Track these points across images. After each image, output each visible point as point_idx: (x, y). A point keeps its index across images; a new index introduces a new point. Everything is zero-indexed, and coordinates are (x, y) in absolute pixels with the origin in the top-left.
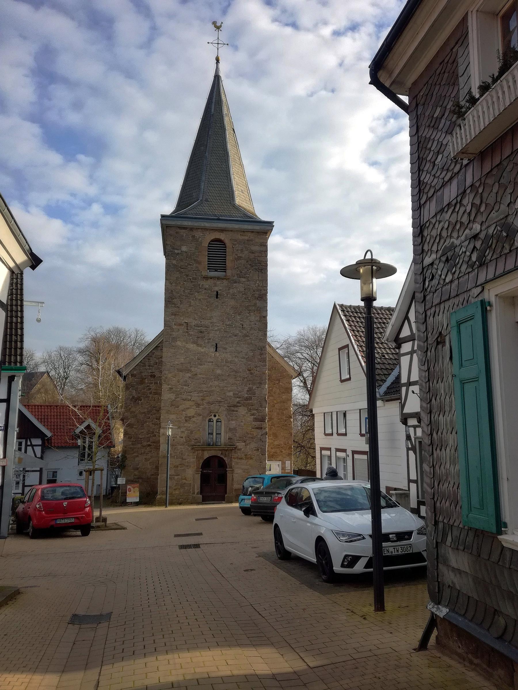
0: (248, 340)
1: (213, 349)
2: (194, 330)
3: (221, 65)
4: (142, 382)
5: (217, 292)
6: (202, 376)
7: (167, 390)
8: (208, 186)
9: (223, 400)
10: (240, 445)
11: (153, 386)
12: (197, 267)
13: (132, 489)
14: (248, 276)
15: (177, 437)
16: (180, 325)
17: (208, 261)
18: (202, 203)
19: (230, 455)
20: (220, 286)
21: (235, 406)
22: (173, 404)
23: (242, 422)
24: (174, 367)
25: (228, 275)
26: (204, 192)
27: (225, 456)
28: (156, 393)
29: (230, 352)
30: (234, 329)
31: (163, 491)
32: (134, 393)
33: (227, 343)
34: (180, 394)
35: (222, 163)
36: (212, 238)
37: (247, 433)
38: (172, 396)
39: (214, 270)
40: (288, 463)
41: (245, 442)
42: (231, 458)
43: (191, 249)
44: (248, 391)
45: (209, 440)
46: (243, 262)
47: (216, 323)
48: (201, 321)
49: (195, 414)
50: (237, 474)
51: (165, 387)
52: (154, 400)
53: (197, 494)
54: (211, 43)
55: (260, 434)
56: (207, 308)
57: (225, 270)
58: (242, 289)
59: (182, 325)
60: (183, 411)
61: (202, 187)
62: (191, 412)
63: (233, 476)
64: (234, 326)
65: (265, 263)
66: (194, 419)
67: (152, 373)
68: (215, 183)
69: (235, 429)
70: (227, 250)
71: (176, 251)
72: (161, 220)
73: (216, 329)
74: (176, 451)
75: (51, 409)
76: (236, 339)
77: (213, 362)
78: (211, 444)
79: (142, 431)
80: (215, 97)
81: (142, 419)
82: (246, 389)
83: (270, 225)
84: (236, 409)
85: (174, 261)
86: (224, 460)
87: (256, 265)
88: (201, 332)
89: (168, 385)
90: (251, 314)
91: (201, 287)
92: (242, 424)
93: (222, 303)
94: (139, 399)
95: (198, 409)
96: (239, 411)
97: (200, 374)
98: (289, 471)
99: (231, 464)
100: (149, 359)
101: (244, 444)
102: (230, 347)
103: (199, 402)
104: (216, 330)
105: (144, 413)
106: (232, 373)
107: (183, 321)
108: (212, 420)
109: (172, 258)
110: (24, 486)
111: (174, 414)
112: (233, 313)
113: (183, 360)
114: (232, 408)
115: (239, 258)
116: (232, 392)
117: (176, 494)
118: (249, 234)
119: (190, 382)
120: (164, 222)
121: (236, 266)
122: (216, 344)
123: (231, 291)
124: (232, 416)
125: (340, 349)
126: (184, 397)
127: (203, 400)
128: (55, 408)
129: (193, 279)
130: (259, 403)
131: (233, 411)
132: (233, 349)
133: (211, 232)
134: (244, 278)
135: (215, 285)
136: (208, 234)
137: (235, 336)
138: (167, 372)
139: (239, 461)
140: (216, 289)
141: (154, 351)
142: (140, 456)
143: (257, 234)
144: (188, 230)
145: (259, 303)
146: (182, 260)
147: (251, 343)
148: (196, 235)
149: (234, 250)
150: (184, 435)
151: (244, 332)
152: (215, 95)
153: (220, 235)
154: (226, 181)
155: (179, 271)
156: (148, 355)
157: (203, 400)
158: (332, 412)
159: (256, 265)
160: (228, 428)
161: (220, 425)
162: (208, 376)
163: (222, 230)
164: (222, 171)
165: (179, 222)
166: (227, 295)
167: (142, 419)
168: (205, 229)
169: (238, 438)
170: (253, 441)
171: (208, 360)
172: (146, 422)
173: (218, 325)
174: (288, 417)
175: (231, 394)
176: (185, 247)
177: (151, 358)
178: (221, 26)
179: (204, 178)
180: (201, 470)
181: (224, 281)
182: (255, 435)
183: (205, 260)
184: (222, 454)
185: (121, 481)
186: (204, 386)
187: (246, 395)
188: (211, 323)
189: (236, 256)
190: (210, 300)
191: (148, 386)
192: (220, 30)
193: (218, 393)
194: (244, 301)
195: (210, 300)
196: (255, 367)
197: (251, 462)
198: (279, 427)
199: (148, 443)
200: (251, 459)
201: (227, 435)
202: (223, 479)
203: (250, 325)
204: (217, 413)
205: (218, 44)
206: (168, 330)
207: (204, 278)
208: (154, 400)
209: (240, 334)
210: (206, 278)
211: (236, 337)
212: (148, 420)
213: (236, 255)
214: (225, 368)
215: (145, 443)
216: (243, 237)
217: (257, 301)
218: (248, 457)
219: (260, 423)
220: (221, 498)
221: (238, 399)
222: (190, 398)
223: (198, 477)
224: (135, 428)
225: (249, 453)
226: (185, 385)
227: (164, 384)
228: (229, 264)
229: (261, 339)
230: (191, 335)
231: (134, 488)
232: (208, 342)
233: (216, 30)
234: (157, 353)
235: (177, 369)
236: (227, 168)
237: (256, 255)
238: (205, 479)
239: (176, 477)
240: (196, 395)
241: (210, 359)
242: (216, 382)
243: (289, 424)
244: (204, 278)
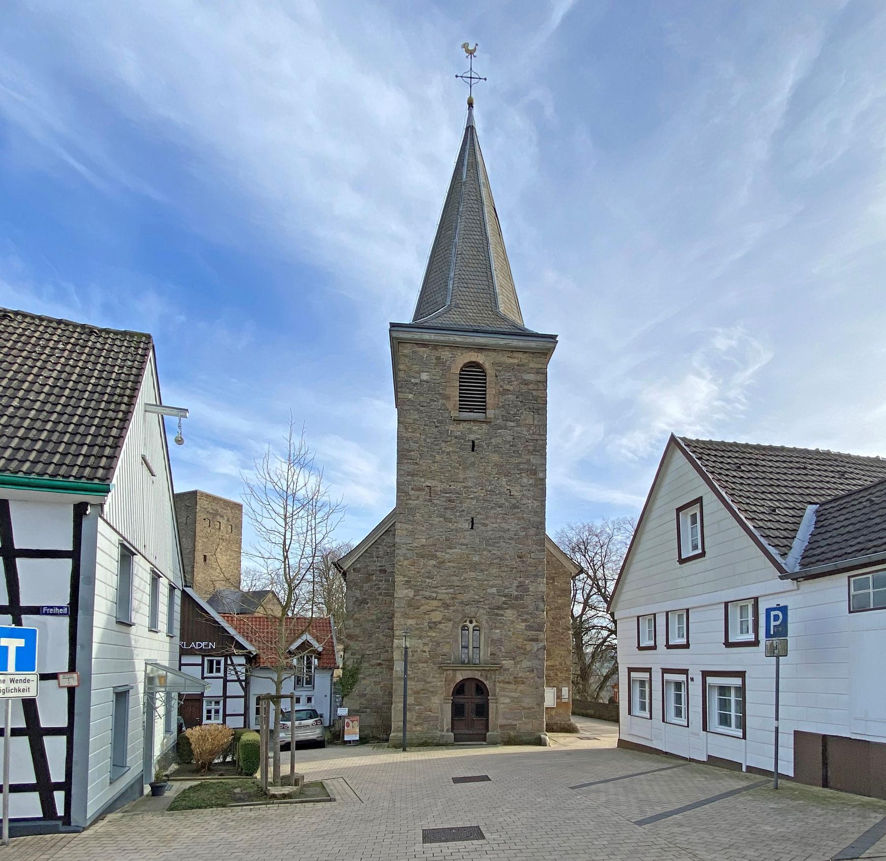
0: (518, 513)
1: (467, 526)
2: (439, 497)
3: (475, 111)
4: (368, 578)
5: (473, 442)
6: (451, 564)
7: (403, 584)
9: (482, 600)
10: (507, 663)
11: (383, 585)
12: (444, 404)
13: (351, 723)
14: (518, 418)
15: (417, 651)
16: (420, 489)
17: (460, 397)
18: (450, 310)
19: (493, 677)
20: (477, 432)
21: (498, 608)
22: (411, 604)
23: (509, 631)
24: (412, 550)
25: (488, 416)
26: (453, 295)
27: (487, 679)
28: (387, 595)
29: (491, 531)
30: (499, 496)
31: (399, 727)
32: (358, 593)
33: (487, 517)
34: (421, 590)
35: (479, 253)
37: (518, 647)
38: (411, 593)
39: (468, 410)
40: (565, 691)
41: (514, 659)
42: (495, 682)
43: (434, 377)
44: (518, 587)
45: (463, 656)
47: (471, 487)
48: (450, 484)
49: (442, 619)
50: (503, 703)
51: (399, 579)
52: (386, 604)
53: (447, 731)
55: (536, 649)
56: (458, 465)
57: (484, 410)
58: (509, 438)
59: (423, 490)
60: (425, 614)
61: (451, 286)
62: (437, 616)
63: (497, 707)
64: (497, 492)
65: (543, 400)
66: (442, 626)
67: (382, 566)
69: (499, 640)
70: (487, 380)
71: (413, 380)
72: (390, 331)
73: (472, 496)
74: (416, 670)
75: (260, 621)
76: (501, 512)
77: (467, 545)
78: (466, 662)
79: (370, 645)
80: (467, 157)
81: (369, 629)
82: (516, 583)
83: (552, 339)
84: (501, 612)
85: (411, 395)
86: (485, 685)
88: (450, 501)
89: (404, 576)
90: (523, 475)
91: (449, 434)
92: (510, 633)
93: (481, 458)
94: (364, 602)
95: (446, 611)
96: (505, 615)
97: (449, 562)
98: (566, 701)
99: (495, 690)
100: (378, 548)
101: (512, 662)
102: (493, 523)
103: (448, 602)
104: (471, 498)
105: (372, 621)
106: (495, 561)
107: (424, 485)
108: (466, 628)
109: (408, 390)
110: (225, 715)
111: (412, 618)
112: (496, 474)
113: (424, 540)
114: (495, 611)
116: (495, 589)
117: (417, 731)
118: (520, 355)
119: (436, 573)
120: (395, 334)
121: (501, 404)
122: (472, 518)
123: (493, 441)
124: (495, 623)
125: (679, 510)
126: (427, 594)
127: (453, 598)
128: (266, 620)
129: (438, 423)
130: (534, 604)
131: (497, 615)
132: (496, 525)
133: (464, 352)
135: (471, 431)
136: (459, 354)
137: (499, 507)
138: (402, 558)
139: (507, 686)
140: (472, 437)
141: (384, 537)
142: (368, 678)
143: (532, 355)
144: (430, 348)
145: (534, 460)
146: (421, 394)
147: (523, 518)
149: (497, 380)
150: (427, 649)
151: (513, 501)
153: (478, 356)
154: (485, 279)
155: (418, 410)
156: (375, 542)
157: (453, 598)
158: (655, 615)
160: (490, 639)
162: (461, 565)
163: (481, 349)
164: (480, 265)
165: (417, 335)
166: (488, 446)
167: (369, 629)
168: (455, 347)
169: (504, 654)
170: (525, 658)
171: (460, 542)
172: (375, 633)
173: (475, 490)
174: (565, 629)
175: (494, 590)
176: (426, 374)
177: (380, 546)
179: (452, 275)
180: (452, 698)
181: (484, 426)
182: (528, 649)
183: (455, 393)
184: (481, 676)
185: (342, 712)
186: (455, 578)
187: (516, 593)
188: (465, 487)
190: (463, 453)
191: (376, 585)
192: (475, 56)
193: (475, 589)
194: (513, 456)
195: (463, 453)
196: (528, 553)
197: (521, 687)
198: (554, 641)
199: (379, 661)
200: (522, 683)
201: (489, 649)
202: (482, 711)
203: (521, 491)
204: (474, 617)
205: (471, 78)
206: (402, 498)
207: (454, 420)
208: (386, 604)
209: (507, 504)
210: (458, 421)
211: (500, 509)
212: (377, 630)
213: (501, 387)
214: (485, 553)
215: (374, 662)
216: (512, 361)
218: (517, 681)
219: (535, 633)
220: (481, 738)
221: (504, 599)
222: (434, 595)
223: (448, 708)
224: (360, 641)
225: (520, 675)
226: (428, 577)
227: (398, 575)
228: (490, 400)
229: (536, 512)
230: (436, 505)
231: (353, 721)
232: (461, 516)
233: (467, 57)
234: (388, 539)
235: (416, 553)
237: (531, 387)
238: (458, 711)
239: (417, 708)
240: (444, 591)
241: (464, 540)
242: (472, 573)
243: (567, 639)
244: (454, 420)
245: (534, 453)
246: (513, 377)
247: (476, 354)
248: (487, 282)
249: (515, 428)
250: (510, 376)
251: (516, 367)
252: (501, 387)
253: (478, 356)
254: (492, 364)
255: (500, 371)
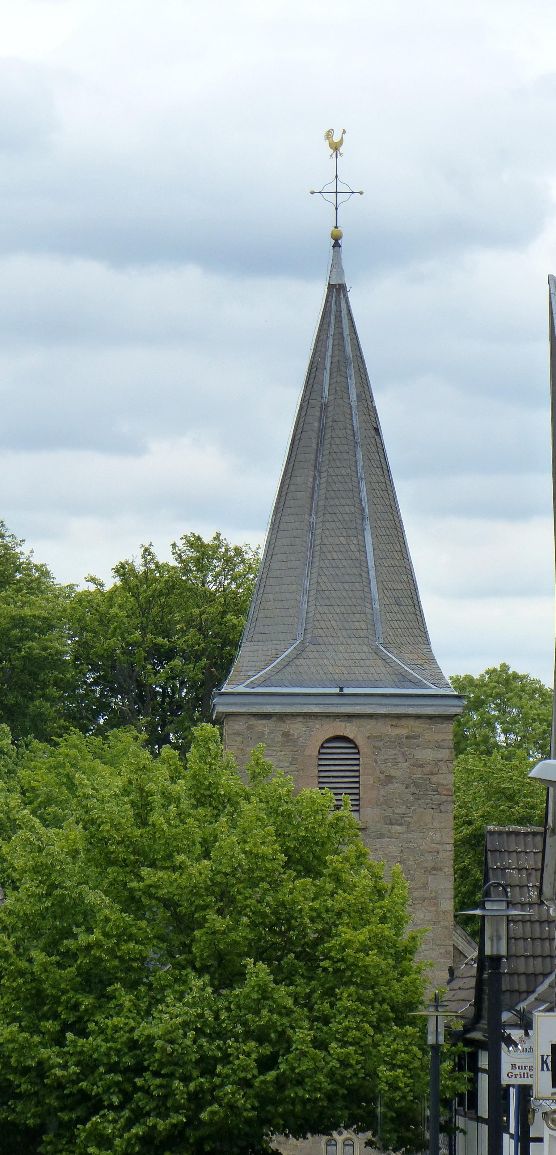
8: (317, 604)
36: (330, 735)
46: (395, 787)
54: (320, 192)
68: (334, 594)
87: (426, 795)
115: (390, 779)
134: (400, 825)
136: (318, 726)
143: (430, 721)
148: (291, 731)
152: (330, 346)
159: (426, 795)
161: (351, 1151)
178: (341, 142)
189: (381, 775)
213: (382, 772)
217: (430, 878)
236: (361, 553)
245: (434, 872)
246: (401, 756)
247: (343, 723)
248: (361, 593)
249: (405, 835)
250: (395, 754)
251: (404, 740)
252: (382, 772)
253: (346, 727)
254: (368, 738)
255: (379, 749)
